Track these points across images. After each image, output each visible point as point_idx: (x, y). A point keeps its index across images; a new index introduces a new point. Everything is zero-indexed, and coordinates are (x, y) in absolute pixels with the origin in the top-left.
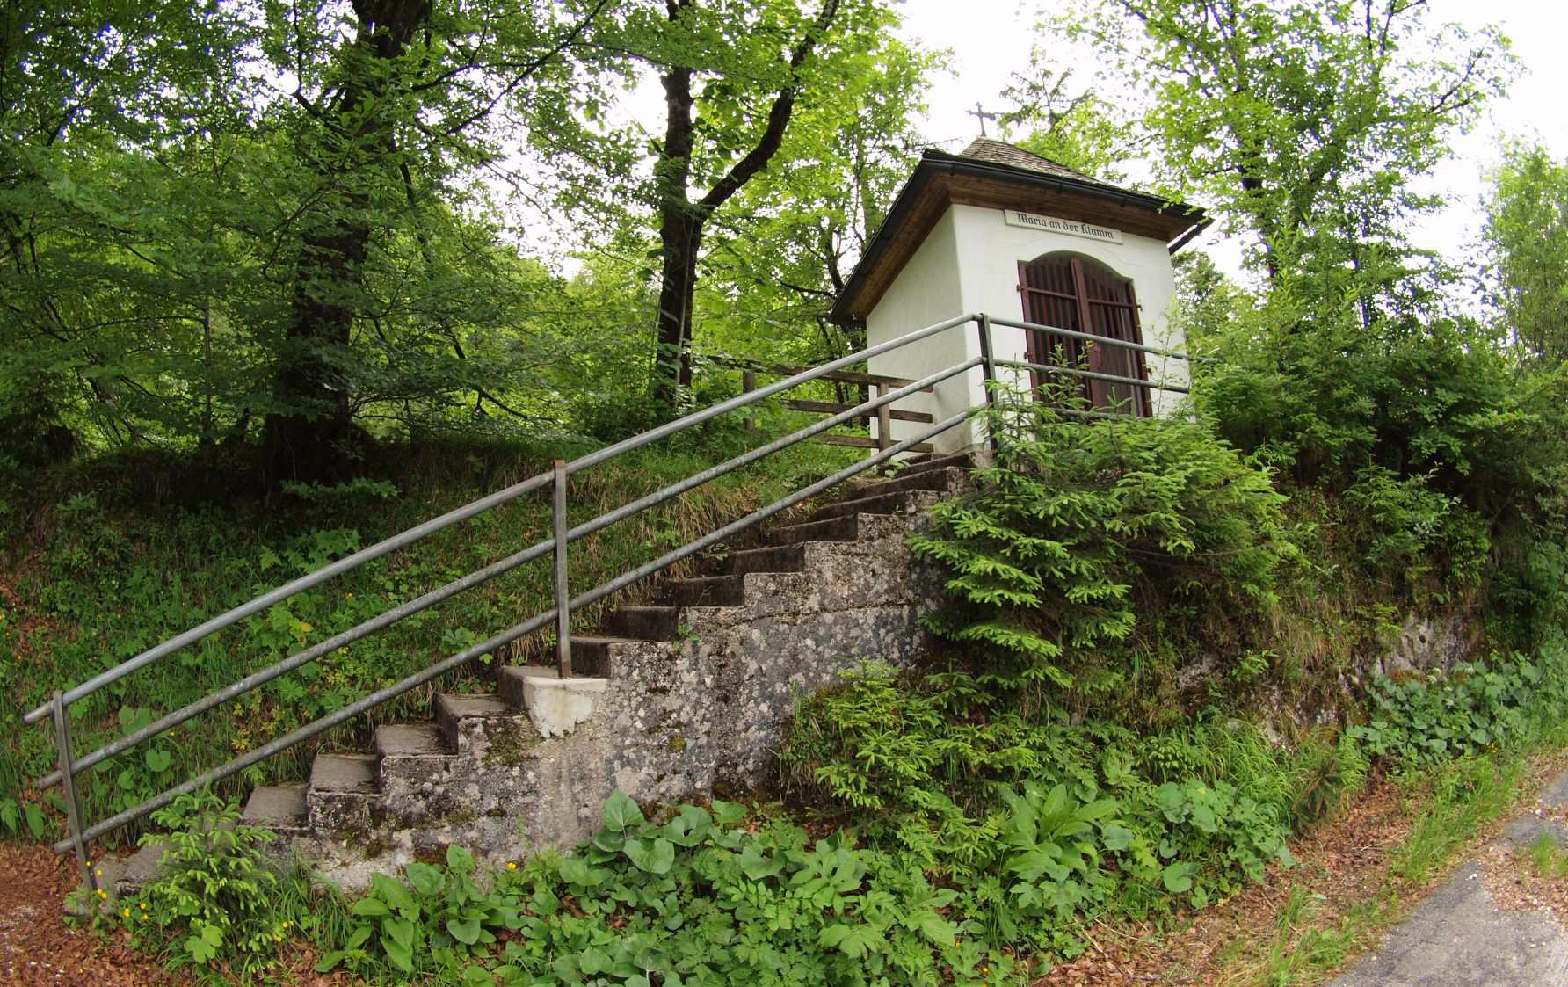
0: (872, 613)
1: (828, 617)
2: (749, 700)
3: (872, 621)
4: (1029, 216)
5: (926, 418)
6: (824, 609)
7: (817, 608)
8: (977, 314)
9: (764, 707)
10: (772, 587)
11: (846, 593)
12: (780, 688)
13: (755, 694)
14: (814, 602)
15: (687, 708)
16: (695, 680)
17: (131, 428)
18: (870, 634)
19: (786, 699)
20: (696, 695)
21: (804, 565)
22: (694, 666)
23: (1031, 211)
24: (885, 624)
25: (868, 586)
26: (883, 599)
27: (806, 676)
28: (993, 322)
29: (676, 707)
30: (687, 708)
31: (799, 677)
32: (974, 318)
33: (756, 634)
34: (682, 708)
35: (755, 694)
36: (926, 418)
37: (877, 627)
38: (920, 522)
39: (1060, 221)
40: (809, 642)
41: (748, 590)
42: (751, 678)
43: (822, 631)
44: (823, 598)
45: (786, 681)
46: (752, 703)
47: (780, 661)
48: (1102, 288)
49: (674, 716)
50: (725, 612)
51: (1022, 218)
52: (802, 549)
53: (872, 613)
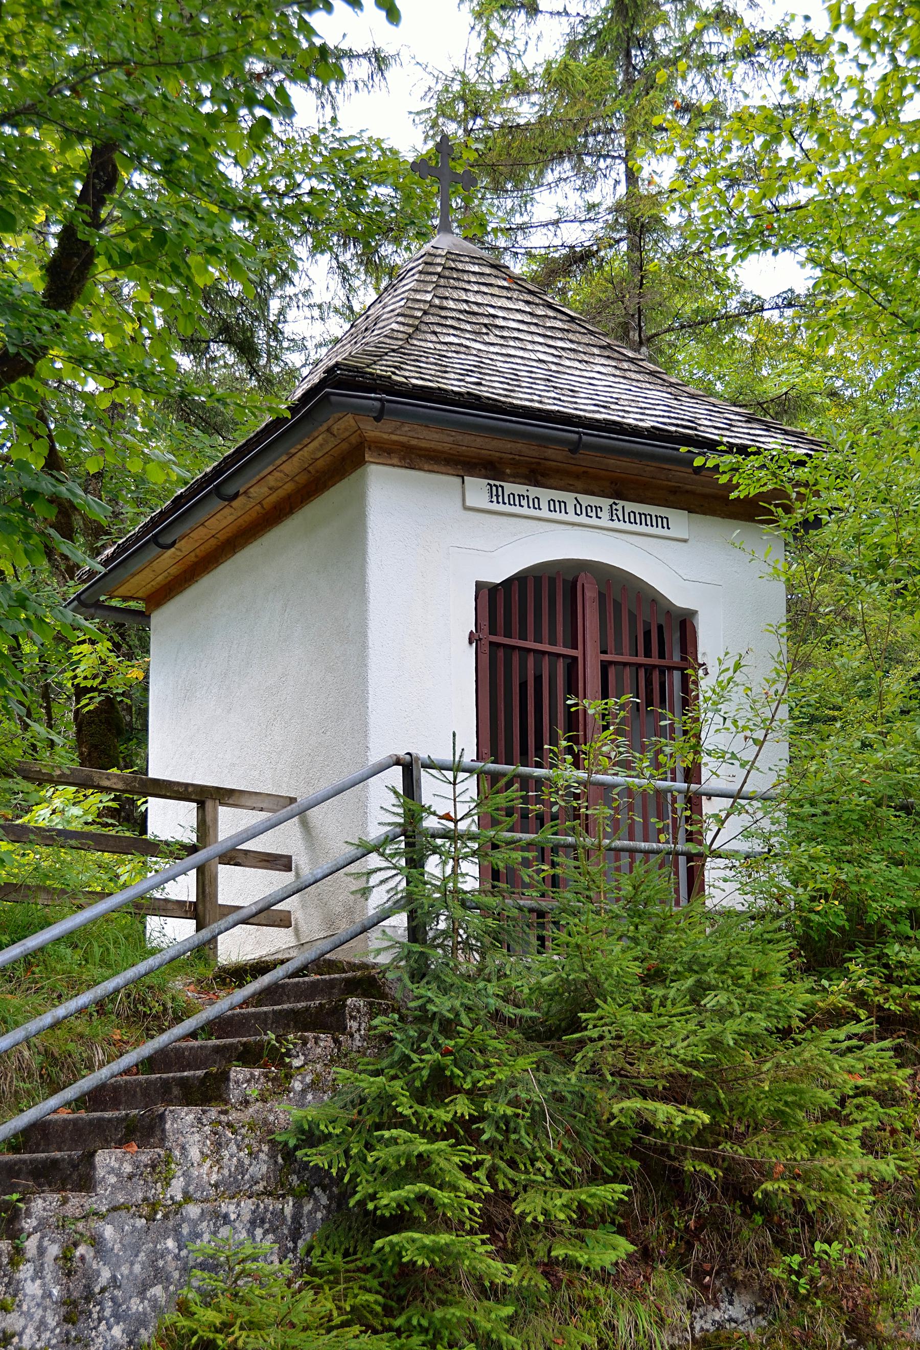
0: (247, 1205)
1: (193, 1211)
2: (100, 1320)
3: (247, 1217)
4: (509, 487)
5: (281, 862)
6: (188, 1198)
7: (179, 1197)
8: (401, 753)
9: (117, 1331)
10: (128, 1168)
11: (214, 1178)
12: (136, 1306)
13: (107, 1313)
14: (176, 1189)
15: (30, 1330)
16: (39, 1293)
17: (585, 970)
18: (243, 1235)
19: (142, 1321)
20: (40, 1312)
21: (163, 1140)
22: (38, 1274)
23: (516, 478)
24: (263, 1221)
25: (241, 1168)
26: (260, 1187)
27: (166, 1289)
28: (425, 766)
29: (18, 1328)
30: (30, 1330)
31: (157, 1291)
32: (398, 763)
33: (109, 1231)
34: (24, 1328)
35: (107, 1313)
36: (281, 862)
37: (253, 1223)
38: (308, 1079)
39: (569, 497)
40: (170, 1244)
41: (100, 1173)
42: (103, 1290)
43: (185, 1230)
44: (188, 1184)
45: (142, 1294)
46: (103, 1327)
47: (137, 1268)
48: (633, 618)
49: (15, 1340)
50: (76, 1202)
51: (496, 495)
52: (162, 1117)
53: (247, 1205)
